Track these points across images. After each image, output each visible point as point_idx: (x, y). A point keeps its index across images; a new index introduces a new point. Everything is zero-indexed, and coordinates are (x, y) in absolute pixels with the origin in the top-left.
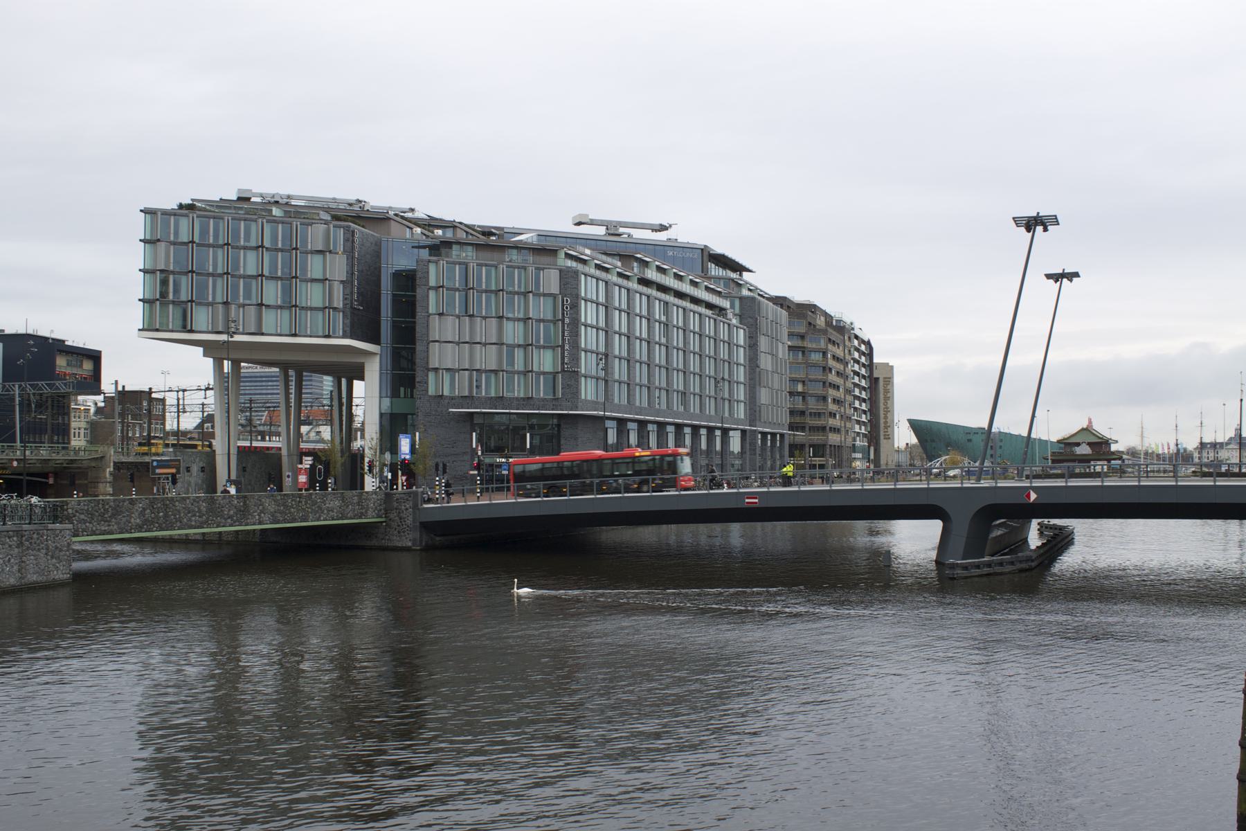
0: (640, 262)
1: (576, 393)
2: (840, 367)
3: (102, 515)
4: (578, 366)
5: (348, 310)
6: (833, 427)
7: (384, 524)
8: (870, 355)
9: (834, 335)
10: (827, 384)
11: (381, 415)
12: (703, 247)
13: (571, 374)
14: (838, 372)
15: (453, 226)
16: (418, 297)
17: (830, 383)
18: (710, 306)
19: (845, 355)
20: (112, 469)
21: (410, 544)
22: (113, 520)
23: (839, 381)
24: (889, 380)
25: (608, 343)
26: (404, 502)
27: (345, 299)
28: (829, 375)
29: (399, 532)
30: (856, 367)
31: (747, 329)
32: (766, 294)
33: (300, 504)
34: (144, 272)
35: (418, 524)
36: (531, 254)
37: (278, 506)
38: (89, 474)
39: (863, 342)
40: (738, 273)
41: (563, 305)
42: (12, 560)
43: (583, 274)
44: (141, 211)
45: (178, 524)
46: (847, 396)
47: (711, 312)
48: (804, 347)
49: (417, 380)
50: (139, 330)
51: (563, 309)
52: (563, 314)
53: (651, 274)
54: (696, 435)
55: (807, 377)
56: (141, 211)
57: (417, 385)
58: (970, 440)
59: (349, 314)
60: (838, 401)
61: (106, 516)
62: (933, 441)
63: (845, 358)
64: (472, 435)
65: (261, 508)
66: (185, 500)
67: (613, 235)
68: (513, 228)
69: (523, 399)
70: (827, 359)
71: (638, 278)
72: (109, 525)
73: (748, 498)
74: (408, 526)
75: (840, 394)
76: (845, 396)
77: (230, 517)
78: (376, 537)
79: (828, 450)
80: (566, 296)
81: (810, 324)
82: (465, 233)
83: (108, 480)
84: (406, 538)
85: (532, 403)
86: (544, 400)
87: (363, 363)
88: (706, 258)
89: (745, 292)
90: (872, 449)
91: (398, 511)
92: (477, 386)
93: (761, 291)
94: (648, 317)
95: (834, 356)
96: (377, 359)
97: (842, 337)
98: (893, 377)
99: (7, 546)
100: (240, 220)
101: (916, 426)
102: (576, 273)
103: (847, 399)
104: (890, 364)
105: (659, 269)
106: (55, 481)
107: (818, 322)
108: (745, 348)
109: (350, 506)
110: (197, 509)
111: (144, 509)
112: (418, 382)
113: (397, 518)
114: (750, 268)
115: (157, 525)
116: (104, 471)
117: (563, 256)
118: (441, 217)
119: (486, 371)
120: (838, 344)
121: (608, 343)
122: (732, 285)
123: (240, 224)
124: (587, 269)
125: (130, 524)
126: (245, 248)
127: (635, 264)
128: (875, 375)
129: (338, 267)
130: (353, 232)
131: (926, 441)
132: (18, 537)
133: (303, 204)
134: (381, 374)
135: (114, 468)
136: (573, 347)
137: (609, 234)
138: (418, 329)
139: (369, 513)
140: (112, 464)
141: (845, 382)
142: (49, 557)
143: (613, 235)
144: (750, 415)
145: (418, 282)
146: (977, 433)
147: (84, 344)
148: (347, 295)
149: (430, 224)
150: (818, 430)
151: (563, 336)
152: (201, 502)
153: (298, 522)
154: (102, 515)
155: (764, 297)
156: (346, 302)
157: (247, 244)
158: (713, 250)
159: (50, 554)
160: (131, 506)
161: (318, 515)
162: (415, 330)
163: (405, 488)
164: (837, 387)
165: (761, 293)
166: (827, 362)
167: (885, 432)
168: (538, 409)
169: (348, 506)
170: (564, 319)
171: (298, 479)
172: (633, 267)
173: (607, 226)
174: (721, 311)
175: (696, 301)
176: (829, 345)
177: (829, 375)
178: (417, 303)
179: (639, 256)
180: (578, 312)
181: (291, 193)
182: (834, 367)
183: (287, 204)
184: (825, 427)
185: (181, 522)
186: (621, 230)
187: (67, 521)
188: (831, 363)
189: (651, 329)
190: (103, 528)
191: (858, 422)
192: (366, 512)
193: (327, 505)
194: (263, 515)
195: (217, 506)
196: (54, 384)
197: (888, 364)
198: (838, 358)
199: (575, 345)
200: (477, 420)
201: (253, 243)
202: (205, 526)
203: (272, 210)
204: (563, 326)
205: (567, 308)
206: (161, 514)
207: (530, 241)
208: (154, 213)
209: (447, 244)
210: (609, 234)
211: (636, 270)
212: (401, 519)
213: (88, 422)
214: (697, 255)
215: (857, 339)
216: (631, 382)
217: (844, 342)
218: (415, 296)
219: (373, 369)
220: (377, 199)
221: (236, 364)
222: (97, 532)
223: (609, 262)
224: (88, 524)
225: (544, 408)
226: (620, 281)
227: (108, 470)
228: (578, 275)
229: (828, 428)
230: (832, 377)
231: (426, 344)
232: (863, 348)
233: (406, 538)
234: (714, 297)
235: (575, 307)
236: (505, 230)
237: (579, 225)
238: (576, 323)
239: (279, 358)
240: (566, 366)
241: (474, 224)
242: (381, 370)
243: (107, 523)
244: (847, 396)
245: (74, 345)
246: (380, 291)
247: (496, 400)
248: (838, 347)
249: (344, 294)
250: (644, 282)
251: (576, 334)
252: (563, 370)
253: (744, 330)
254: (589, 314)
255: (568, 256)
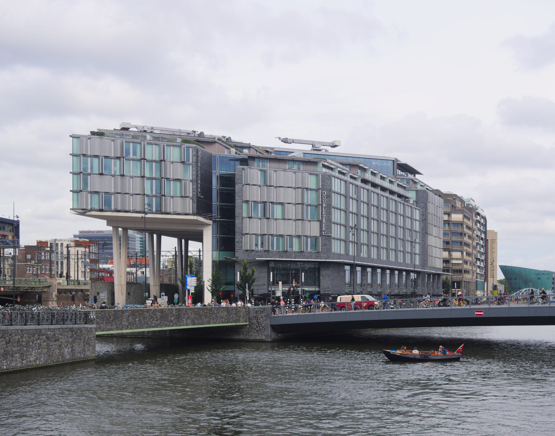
0: (361, 169)
1: (330, 249)
2: (470, 233)
3: (108, 319)
4: (331, 233)
5: (195, 198)
6: (466, 270)
7: (248, 326)
8: (485, 226)
9: (468, 214)
10: (463, 244)
11: (213, 262)
12: (394, 159)
13: (328, 238)
14: (469, 236)
15: (256, 149)
16: (237, 190)
17: (465, 243)
18: (400, 196)
19: (473, 225)
20: (56, 293)
21: (264, 338)
22: (114, 322)
23: (469, 241)
24: (494, 241)
25: (347, 219)
26: (260, 313)
27: (193, 191)
28: (465, 238)
29: (257, 331)
30: (479, 233)
31: (421, 210)
32: (430, 188)
33: (206, 314)
34: (73, 174)
35: (269, 326)
36: (268, 162)
37: (195, 315)
38: (43, 296)
39: (482, 217)
40: (413, 175)
41: (322, 196)
42: (69, 345)
43: (333, 177)
44: (70, 136)
45: (146, 325)
46: (474, 251)
47: (401, 199)
48: (449, 221)
49: (236, 240)
50: (71, 209)
51: (322, 198)
52: (322, 201)
53: (368, 176)
54: (353, 272)
55: (451, 239)
56: (70, 136)
57: (236, 244)
58: (539, 279)
59: (196, 200)
60: (469, 254)
61: (110, 320)
62: (515, 279)
63: (473, 227)
64: (270, 275)
65: (187, 316)
66: (149, 311)
67: (316, 150)
68: (279, 148)
69: (298, 252)
70: (463, 228)
71: (361, 179)
72: (112, 325)
73: (476, 312)
74: (263, 327)
75: (470, 250)
76: (472, 251)
77: (172, 321)
78: (243, 333)
79: (463, 284)
80: (323, 190)
81: (453, 206)
82: (256, 151)
83: (54, 300)
84: (262, 334)
85: (303, 255)
86: (310, 253)
87: (203, 230)
88: (396, 166)
89: (419, 187)
90: (486, 283)
91: (256, 318)
92: (121, 238)
93: (428, 186)
94: (368, 203)
95: (467, 226)
96: (211, 227)
97: (471, 215)
98: (497, 239)
99: (66, 337)
100: (130, 142)
101: (504, 269)
102: (330, 176)
103: (474, 252)
104: (495, 231)
105: (373, 174)
106: (21, 300)
107: (457, 205)
108: (419, 221)
109: (231, 315)
110: (155, 317)
111: (129, 316)
112: (237, 242)
113: (256, 323)
114: (421, 172)
115: (135, 326)
116: (52, 294)
117: (321, 165)
118: (241, 142)
119: (277, 236)
120: (469, 219)
121: (347, 219)
122: (411, 183)
123: (130, 145)
124: (333, 173)
125: (122, 325)
126: (133, 160)
127: (359, 171)
128: (487, 239)
129: (189, 174)
130: (197, 151)
131: (511, 279)
132: (71, 331)
133: (159, 132)
134: (213, 237)
135: (57, 293)
136: (328, 221)
137: (314, 150)
138: (236, 210)
139: (241, 320)
140: (56, 290)
141: (472, 242)
142: (85, 344)
143: (316, 150)
144: (422, 262)
145: (236, 181)
146: (544, 274)
147: (9, 217)
148: (195, 189)
149: (240, 147)
150: (457, 272)
151: (322, 214)
152: (157, 313)
153: (205, 324)
154: (108, 319)
155: (429, 190)
156: (194, 193)
157: (134, 157)
158: (400, 161)
159: (86, 342)
160: (122, 314)
161: (215, 320)
162: (235, 210)
163: (253, 305)
164: (467, 245)
165: (427, 187)
166: (463, 230)
167: (280, 270)
168: (307, 259)
169: (230, 315)
170: (322, 204)
171: (19, 302)
172: (358, 172)
173: (312, 145)
174: (406, 198)
175: (392, 193)
176: (465, 219)
177: (465, 238)
178: (236, 194)
179: (361, 165)
180: (331, 200)
181: (153, 126)
182: (467, 233)
183: (152, 132)
184: (462, 270)
185: (147, 324)
186: (322, 147)
187: (90, 323)
188: (466, 230)
189: (369, 210)
190: (108, 327)
191: (479, 267)
192: (239, 319)
193: (220, 315)
194: (188, 320)
195: (165, 314)
196: (6, 241)
197: (494, 231)
198: (469, 227)
199: (329, 220)
200: (272, 265)
201: (138, 157)
202: (159, 326)
203: (146, 136)
204: (322, 209)
205: (324, 197)
206: (137, 319)
207: (299, 156)
208: (79, 138)
209: (252, 158)
210: (314, 150)
211: (359, 174)
212: (258, 323)
213: (9, 264)
214: (390, 164)
215: (479, 216)
216: (358, 243)
217: (473, 218)
218: (234, 190)
219: (208, 234)
220: (210, 132)
221: (125, 230)
222: (106, 329)
223: (346, 169)
224: (101, 325)
225: (310, 257)
226: (352, 181)
227: (54, 293)
228: (330, 177)
229: (463, 271)
230: (466, 239)
231: (241, 219)
232: (482, 221)
233: (262, 334)
234: (402, 190)
235: (329, 196)
236: (275, 149)
237: (286, 143)
238: (329, 207)
239: (169, 228)
240: (323, 233)
241: (259, 146)
242: (213, 234)
243: (110, 324)
244: (474, 251)
245: (3, 217)
246: (212, 187)
247: (282, 253)
248: (469, 221)
249: (193, 189)
250: (364, 181)
251: (329, 214)
252: (321, 235)
253: (419, 210)
254: (337, 201)
255: (324, 166)
